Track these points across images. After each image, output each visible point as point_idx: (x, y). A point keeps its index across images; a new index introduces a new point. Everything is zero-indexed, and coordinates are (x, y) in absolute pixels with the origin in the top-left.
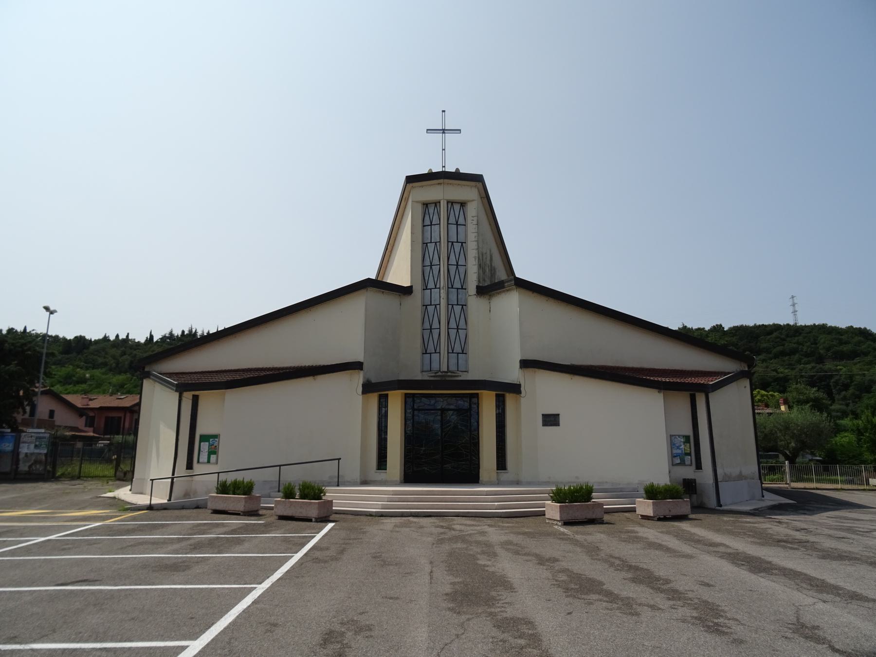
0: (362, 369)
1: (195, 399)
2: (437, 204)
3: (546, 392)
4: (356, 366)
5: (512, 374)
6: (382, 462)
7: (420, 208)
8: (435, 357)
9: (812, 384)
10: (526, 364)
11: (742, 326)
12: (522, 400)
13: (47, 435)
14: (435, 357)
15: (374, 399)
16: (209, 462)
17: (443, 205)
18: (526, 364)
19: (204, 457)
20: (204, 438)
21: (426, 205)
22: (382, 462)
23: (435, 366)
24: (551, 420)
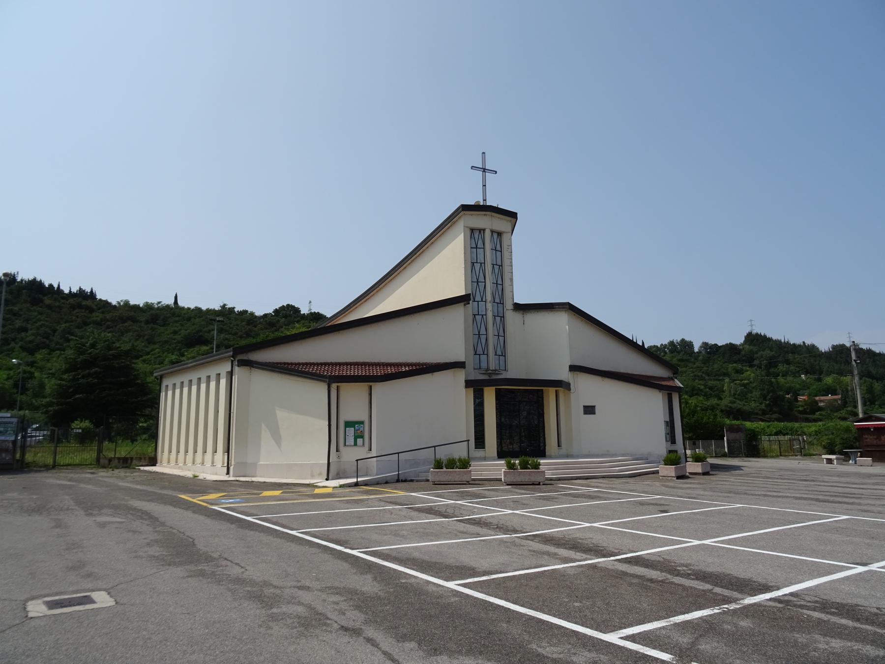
0: (464, 367)
1: (557, 392)
2: (482, 231)
3: (587, 389)
4: (460, 365)
5: (564, 374)
6: (480, 442)
7: (468, 232)
8: (484, 358)
9: (28, 365)
10: (574, 368)
11: (226, 312)
12: (572, 396)
13: (15, 420)
14: (484, 358)
15: (471, 391)
16: (355, 444)
17: (488, 234)
18: (574, 368)
19: (350, 440)
20: (348, 424)
21: (472, 230)
22: (480, 442)
23: (484, 365)
24: (589, 410)
